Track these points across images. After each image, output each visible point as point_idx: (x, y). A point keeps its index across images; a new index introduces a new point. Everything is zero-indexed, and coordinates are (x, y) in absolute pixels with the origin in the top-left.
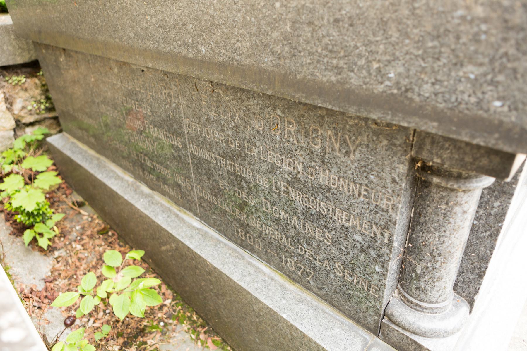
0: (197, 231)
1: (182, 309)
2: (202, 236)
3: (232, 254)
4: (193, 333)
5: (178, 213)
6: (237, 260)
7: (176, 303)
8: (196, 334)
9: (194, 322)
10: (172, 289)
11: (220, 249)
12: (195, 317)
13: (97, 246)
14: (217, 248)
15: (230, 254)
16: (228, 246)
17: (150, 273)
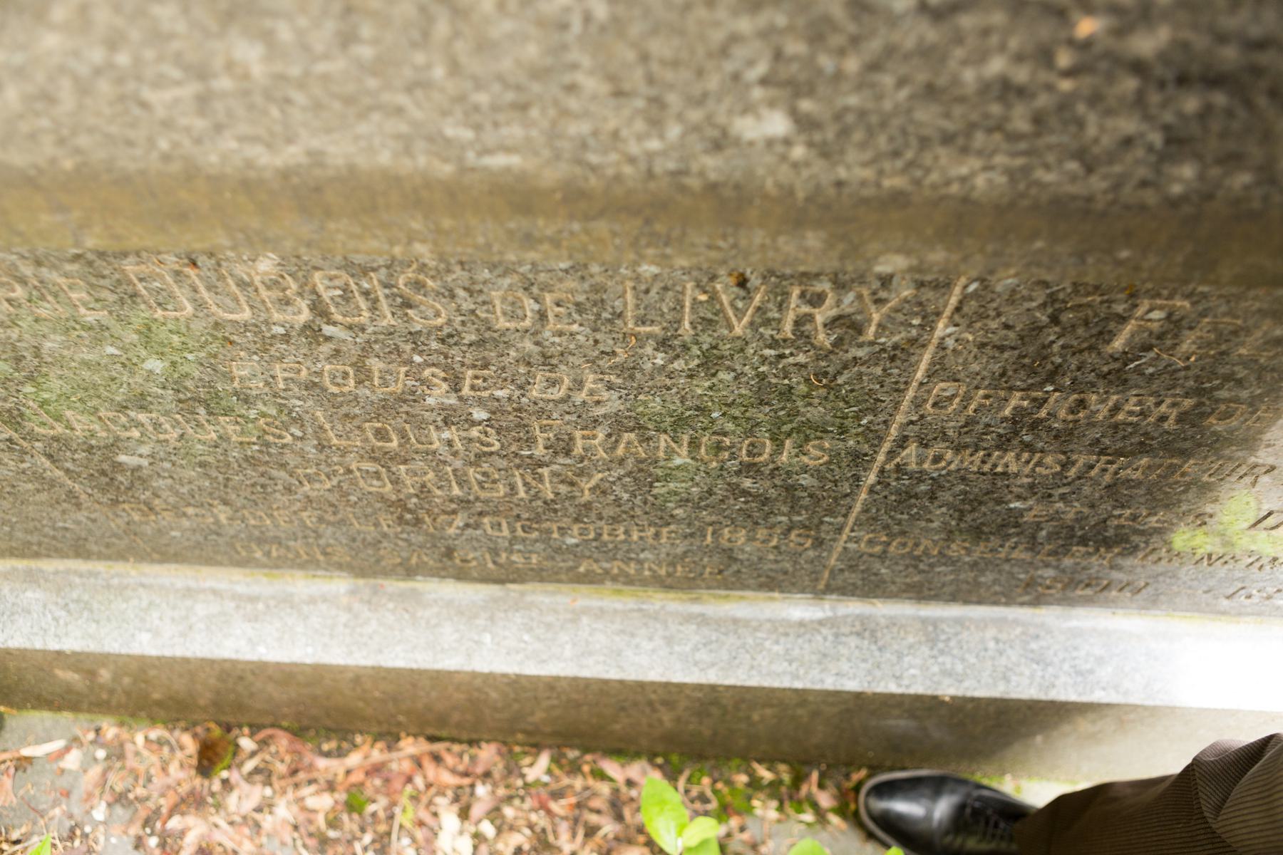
0: (824, 631)
1: (715, 781)
2: (858, 634)
3: (1003, 636)
4: (800, 811)
5: (696, 609)
6: (1034, 646)
7: (689, 780)
8: (806, 806)
9: (775, 785)
10: (636, 755)
11: (953, 643)
12: (766, 774)
13: (258, 816)
14: (941, 645)
15: (997, 641)
16: (971, 619)
17: (527, 760)
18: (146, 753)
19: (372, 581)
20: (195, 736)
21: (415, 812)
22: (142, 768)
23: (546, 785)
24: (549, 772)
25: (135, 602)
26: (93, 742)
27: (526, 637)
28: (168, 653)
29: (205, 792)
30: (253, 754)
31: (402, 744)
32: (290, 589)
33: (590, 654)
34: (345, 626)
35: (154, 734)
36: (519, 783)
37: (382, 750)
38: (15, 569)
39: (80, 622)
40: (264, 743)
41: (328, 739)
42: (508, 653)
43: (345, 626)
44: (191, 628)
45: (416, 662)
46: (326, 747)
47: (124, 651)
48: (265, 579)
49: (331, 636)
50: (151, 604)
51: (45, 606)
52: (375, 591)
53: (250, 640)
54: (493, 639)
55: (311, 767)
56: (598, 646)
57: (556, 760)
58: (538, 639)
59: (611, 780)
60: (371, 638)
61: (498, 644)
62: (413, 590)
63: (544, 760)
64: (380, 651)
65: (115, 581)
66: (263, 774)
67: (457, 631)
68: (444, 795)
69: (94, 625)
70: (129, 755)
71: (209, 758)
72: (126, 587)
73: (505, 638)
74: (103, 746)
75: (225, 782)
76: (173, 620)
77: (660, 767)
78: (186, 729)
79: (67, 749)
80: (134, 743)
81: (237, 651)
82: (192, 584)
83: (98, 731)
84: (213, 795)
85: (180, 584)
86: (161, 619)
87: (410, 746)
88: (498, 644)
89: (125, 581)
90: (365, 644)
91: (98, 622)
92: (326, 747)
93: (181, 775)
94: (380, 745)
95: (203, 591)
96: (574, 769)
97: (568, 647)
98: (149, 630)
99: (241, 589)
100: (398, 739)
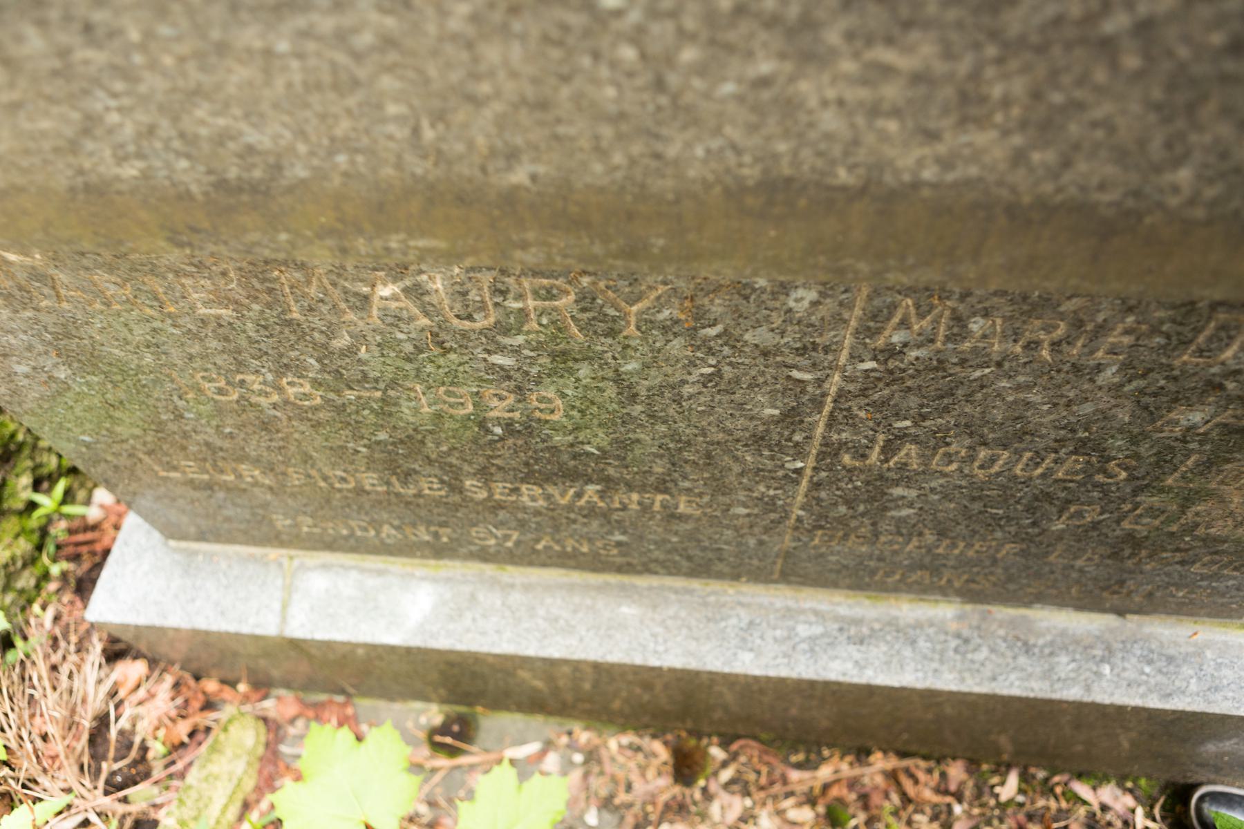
18: (621, 759)
19: (980, 607)
20: (666, 743)
21: (194, 713)
22: (620, 774)
23: (1021, 805)
24: (1021, 791)
25: (734, 621)
26: (569, 746)
27: (1147, 669)
28: (772, 673)
29: (688, 800)
30: (724, 764)
31: (872, 759)
32: (894, 612)
33: (1217, 689)
34: (956, 650)
35: (626, 739)
36: (992, 802)
37: (851, 764)
38: (608, 584)
39: (679, 639)
40: (734, 757)
41: (797, 752)
42: (1129, 685)
43: (956, 650)
44: (794, 648)
45: (1032, 690)
46: (794, 759)
47: (727, 670)
48: (867, 602)
49: (942, 662)
50: (751, 623)
51: (642, 622)
52: (985, 617)
53: (857, 662)
54: (1112, 670)
55: (785, 780)
56: (1225, 682)
57: (1025, 778)
58: (1160, 671)
59: (1085, 803)
60: (983, 665)
61: (1118, 675)
62: (1024, 617)
63: (1013, 780)
64: (994, 679)
65: (712, 599)
66: (739, 785)
67: (1074, 660)
68: (922, 812)
69: (694, 644)
70: (606, 759)
71: (685, 767)
72: (724, 605)
73: (1124, 669)
74: (578, 750)
75: (705, 790)
76: (775, 640)
77: (1131, 791)
78: (654, 736)
79: (543, 753)
80: (607, 748)
81: (844, 674)
82: (791, 603)
83: (570, 733)
84: (695, 803)
85: (779, 604)
86: (762, 638)
87: (880, 762)
88: (1118, 675)
89: (723, 599)
90: (978, 671)
91: (697, 639)
92: (794, 759)
93: (661, 785)
94: (849, 758)
95: (803, 611)
96: (1048, 790)
97: (1193, 681)
98: (751, 650)
99: (843, 611)
100: (868, 753)
